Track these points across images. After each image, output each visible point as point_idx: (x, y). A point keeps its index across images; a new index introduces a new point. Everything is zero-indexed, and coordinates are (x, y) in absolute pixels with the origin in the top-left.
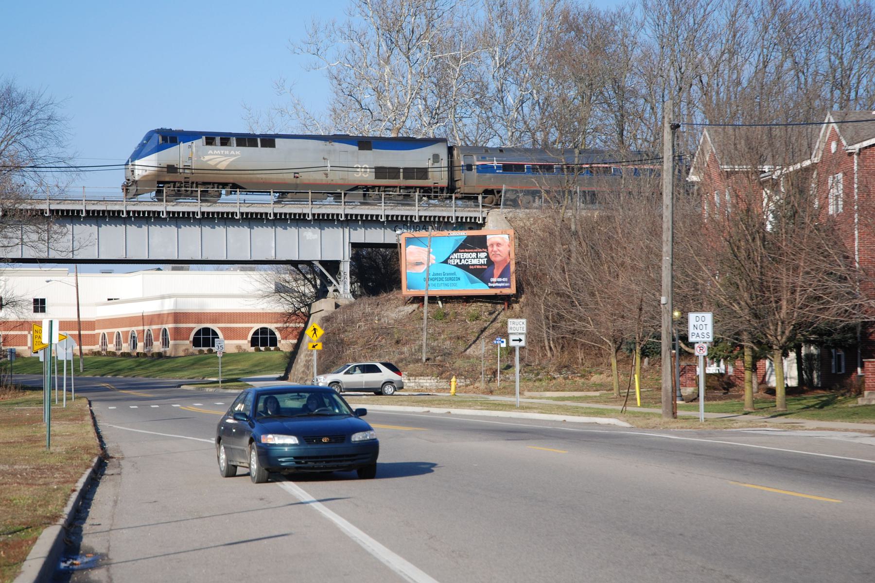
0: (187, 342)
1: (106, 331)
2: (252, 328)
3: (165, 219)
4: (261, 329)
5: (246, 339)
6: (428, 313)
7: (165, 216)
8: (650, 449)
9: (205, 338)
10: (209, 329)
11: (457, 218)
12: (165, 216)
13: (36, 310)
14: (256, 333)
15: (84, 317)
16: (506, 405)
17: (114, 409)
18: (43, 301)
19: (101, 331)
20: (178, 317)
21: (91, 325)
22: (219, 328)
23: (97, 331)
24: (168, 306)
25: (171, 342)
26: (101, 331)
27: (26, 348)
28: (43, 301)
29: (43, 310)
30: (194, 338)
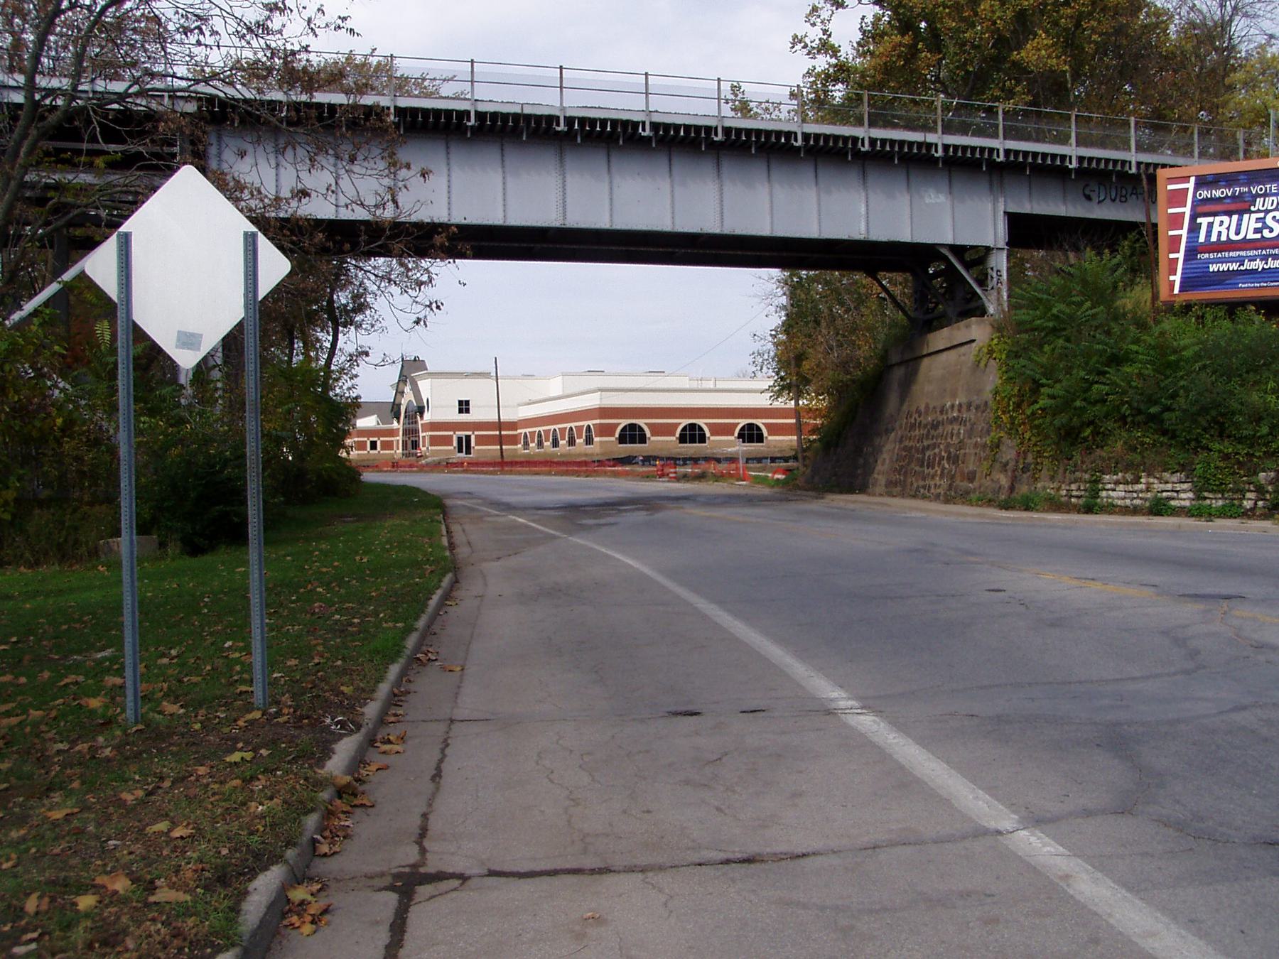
0: (613, 439)
1: (527, 430)
2: (680, 424)
3: (649, 139)
4: (630, 425)
5: (674, 435)
6: (1040, 409)
7: (648, 133)
8: (648, 477)
9: (693, 434)
10: (635, 425)
11: (1139, 164)
12: (648, 133)
13: (461, 411)
14: (684, 429)
15: (503, 419)
16: (585, 463)
17: (746, 485)
18: (467, 403)
19: (523, 431)
20: (604, 412)
21: (513, 425)
22: (646, 424)
23: (519, 431)
24: (592, 401)
25: (596, 439)
26: (522, 431)
27: (452, 448)
28: (467, 403)
29: (467, 411)
30: (620, 435)
